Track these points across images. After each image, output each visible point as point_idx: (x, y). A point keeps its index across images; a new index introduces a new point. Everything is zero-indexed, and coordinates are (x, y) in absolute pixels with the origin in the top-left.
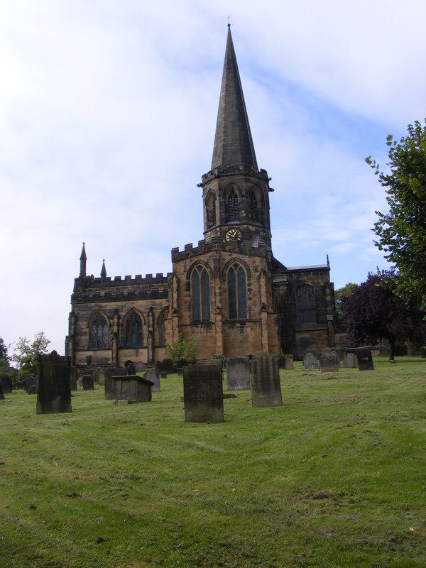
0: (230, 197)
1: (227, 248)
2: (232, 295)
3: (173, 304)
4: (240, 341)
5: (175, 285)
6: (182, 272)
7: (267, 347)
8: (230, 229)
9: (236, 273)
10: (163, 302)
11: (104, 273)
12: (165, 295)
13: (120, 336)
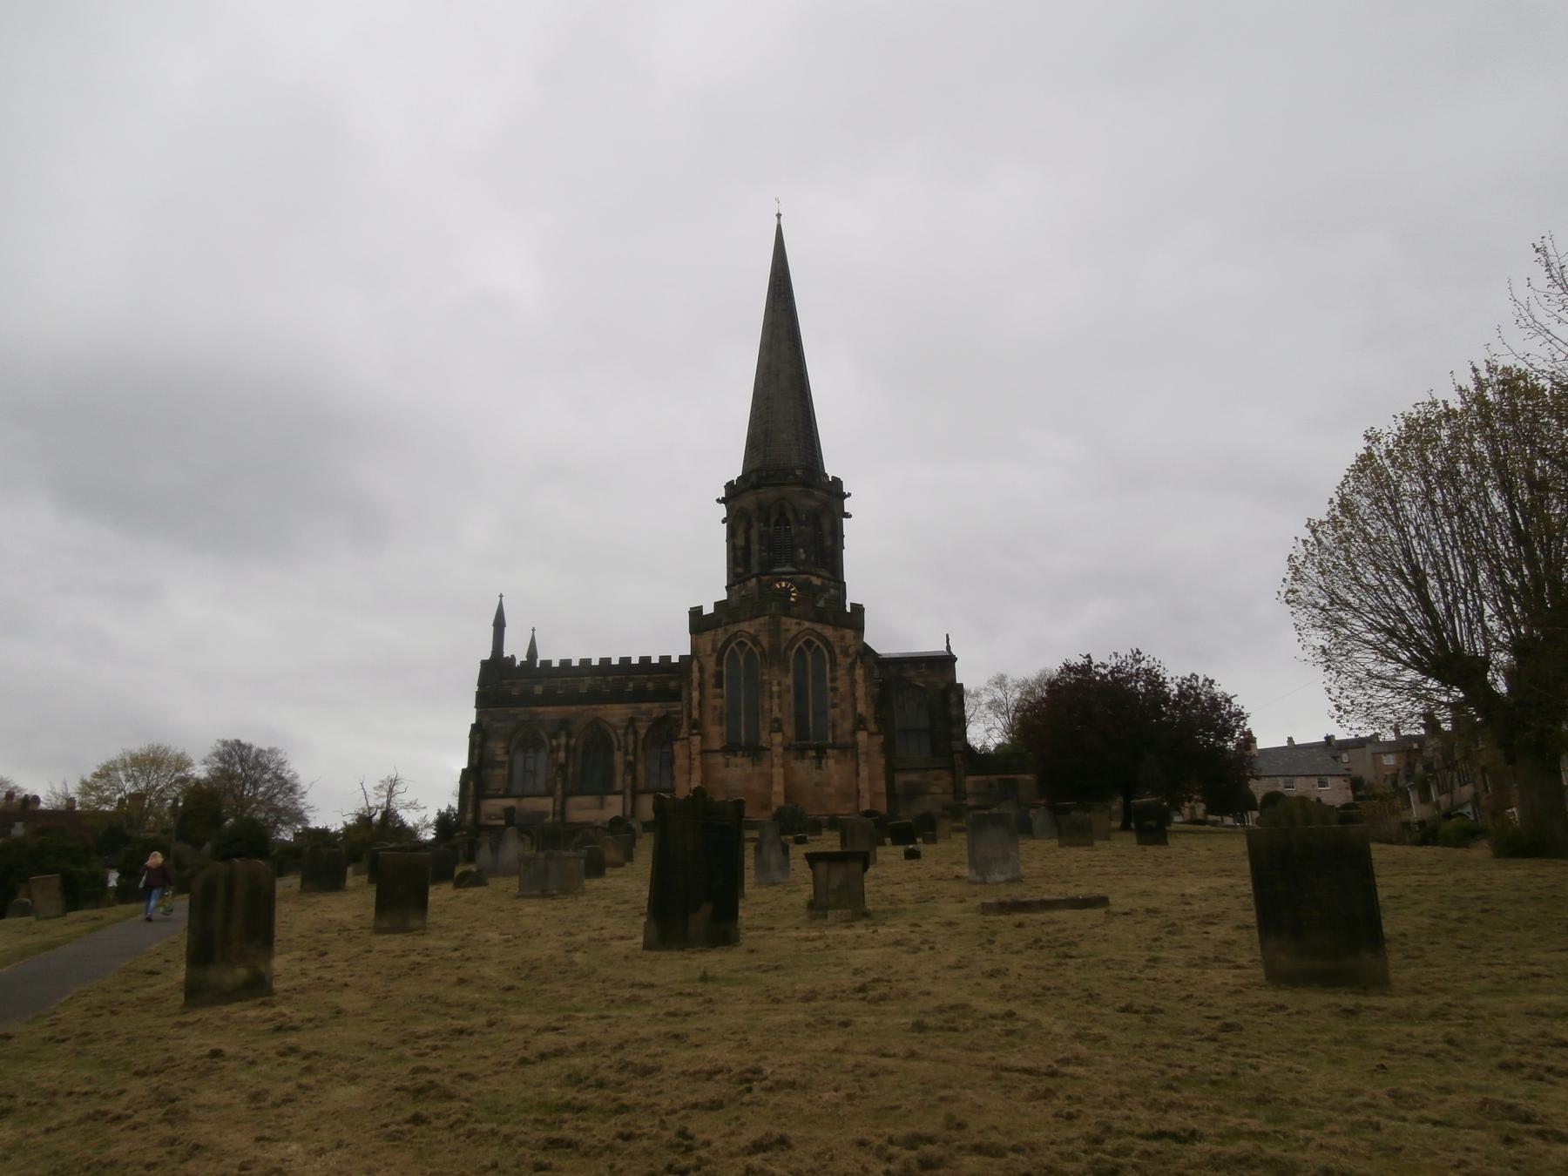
0: (777, 523)
7: (867, 796)
13: (571, 770)
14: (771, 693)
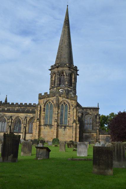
1: (62, 96)
2: (62, 115)
3: (37, 116)
4: (64, 134)
5: (39, 109)
6: (42, 104)
8: (60, 89)
9: (64, 106)
10: (31, 115)
11: (6, 101)
12: (33, 112)
13: (12, 127)
14: (55, 113)
